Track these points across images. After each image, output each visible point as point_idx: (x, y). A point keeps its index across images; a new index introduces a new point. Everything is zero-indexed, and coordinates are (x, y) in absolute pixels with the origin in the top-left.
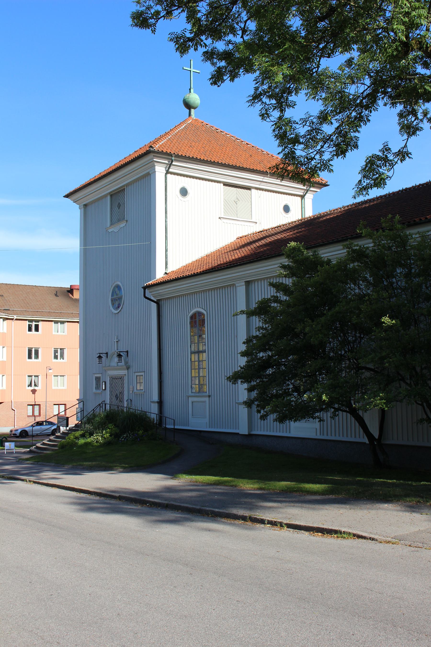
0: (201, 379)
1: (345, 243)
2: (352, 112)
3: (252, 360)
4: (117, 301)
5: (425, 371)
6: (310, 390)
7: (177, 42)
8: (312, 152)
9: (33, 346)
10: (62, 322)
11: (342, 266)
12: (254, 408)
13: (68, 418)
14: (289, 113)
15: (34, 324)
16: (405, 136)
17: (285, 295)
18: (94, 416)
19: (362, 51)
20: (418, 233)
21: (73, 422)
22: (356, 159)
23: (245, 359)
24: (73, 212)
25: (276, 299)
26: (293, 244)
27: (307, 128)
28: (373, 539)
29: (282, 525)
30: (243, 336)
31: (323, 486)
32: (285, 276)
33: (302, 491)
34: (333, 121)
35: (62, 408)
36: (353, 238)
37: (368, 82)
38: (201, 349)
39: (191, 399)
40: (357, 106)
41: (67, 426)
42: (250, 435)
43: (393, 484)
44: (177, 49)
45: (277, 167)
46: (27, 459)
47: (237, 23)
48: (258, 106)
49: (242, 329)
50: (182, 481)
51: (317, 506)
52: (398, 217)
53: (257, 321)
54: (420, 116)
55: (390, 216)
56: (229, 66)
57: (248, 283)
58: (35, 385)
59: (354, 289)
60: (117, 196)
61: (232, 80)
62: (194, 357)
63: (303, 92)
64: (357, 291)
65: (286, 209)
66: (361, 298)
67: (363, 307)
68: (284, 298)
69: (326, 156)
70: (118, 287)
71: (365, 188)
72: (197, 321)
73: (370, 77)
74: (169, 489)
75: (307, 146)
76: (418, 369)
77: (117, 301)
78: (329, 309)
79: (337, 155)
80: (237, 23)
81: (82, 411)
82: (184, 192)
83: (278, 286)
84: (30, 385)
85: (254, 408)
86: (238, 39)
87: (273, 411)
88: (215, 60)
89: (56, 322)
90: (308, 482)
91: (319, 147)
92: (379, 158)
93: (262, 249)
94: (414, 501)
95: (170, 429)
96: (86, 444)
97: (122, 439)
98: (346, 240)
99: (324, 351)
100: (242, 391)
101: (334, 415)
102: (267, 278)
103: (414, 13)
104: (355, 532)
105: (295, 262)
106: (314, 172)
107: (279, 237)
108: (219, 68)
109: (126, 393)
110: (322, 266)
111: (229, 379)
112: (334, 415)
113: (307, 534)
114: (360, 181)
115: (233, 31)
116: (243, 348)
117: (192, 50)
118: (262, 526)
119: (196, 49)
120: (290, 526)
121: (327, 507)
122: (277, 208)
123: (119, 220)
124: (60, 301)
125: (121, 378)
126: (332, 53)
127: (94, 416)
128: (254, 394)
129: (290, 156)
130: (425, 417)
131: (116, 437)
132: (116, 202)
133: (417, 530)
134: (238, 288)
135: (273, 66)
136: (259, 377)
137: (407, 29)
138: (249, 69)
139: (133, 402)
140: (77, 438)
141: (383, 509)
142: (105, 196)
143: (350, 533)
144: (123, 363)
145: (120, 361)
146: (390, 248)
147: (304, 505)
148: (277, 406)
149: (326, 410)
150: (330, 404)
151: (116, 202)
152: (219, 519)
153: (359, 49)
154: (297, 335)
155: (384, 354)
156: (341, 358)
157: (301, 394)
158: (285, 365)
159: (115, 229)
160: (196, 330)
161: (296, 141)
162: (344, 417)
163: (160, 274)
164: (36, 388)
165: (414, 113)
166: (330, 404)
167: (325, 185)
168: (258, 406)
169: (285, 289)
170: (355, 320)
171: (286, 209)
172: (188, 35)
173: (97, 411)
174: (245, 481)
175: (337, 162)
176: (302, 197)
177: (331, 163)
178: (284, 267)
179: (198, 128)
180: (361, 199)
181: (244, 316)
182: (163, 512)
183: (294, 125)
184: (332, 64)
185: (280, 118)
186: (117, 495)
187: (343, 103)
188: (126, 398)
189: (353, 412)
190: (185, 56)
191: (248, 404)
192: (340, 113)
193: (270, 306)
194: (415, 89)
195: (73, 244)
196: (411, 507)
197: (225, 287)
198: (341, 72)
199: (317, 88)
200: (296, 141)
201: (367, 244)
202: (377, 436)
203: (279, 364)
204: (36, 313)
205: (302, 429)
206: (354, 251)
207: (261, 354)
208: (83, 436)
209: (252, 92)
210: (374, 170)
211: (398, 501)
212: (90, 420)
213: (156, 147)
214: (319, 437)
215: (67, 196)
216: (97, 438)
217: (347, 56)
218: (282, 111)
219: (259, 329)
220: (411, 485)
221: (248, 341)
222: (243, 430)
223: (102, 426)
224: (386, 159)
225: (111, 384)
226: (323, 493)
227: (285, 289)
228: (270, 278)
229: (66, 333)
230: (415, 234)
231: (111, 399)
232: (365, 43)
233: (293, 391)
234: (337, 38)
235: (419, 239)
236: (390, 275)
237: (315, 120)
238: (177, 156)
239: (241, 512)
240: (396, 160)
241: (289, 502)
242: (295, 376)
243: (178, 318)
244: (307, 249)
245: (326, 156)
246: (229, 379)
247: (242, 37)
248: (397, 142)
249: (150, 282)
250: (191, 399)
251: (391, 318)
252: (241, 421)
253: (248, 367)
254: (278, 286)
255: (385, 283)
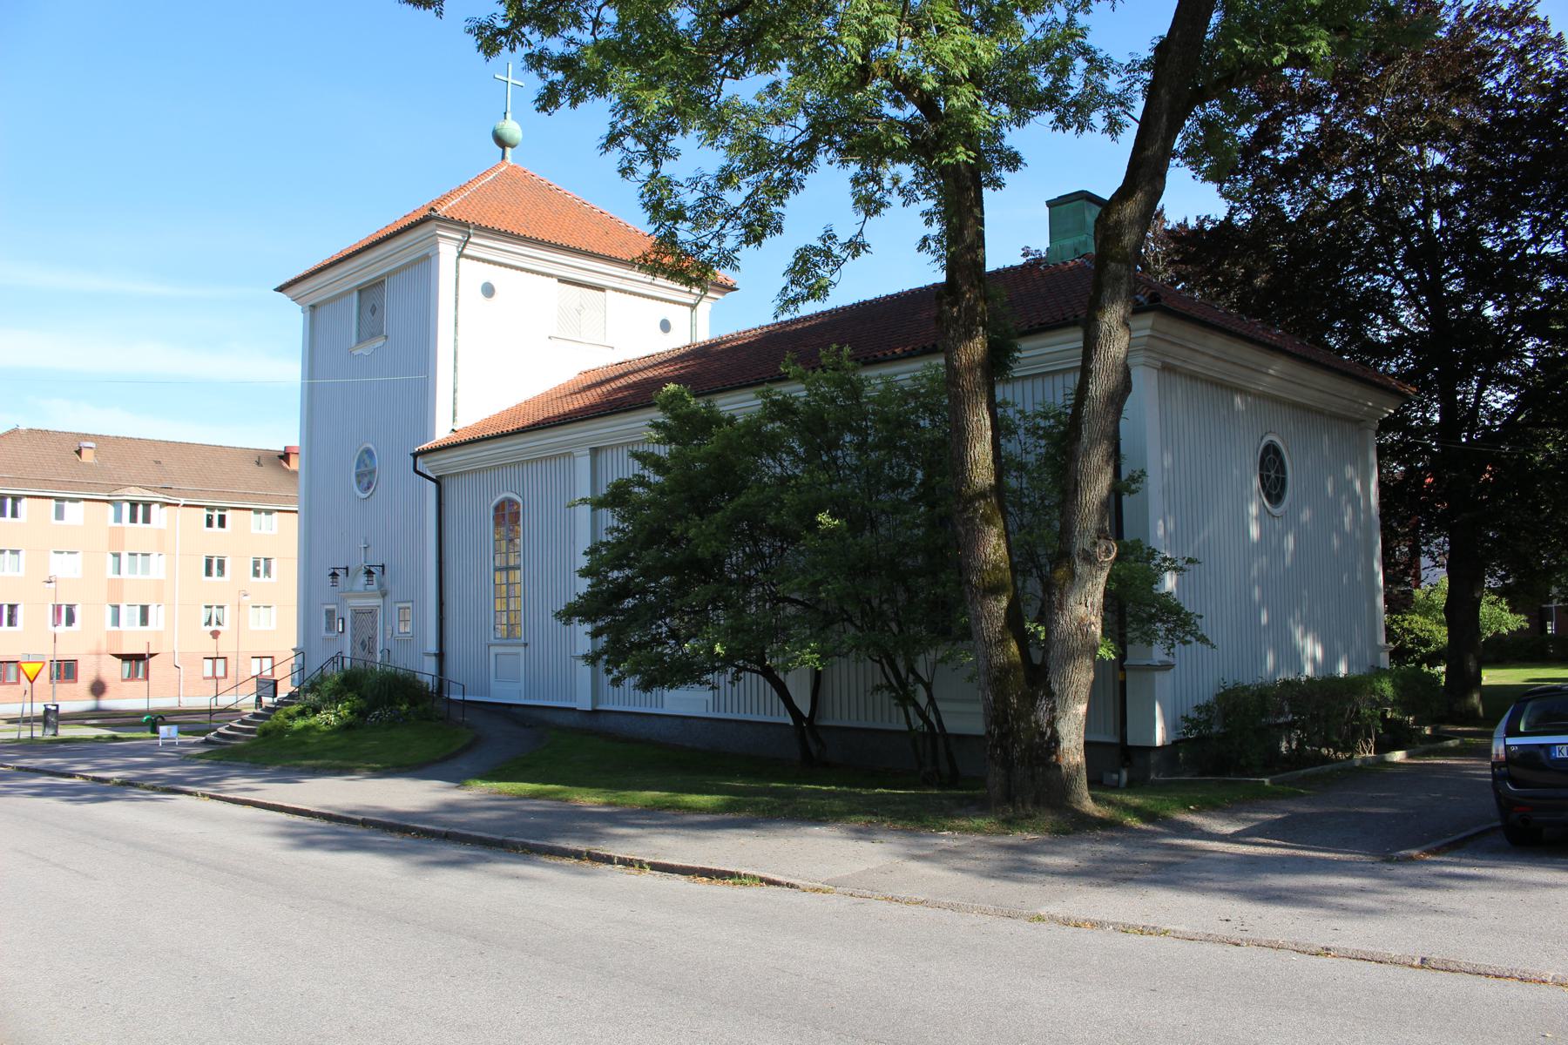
0: (512, 615)
1: (760, 389)
2: (777, 170)
3: (600, 583)
4: (366, 477)
5: (885, 606)
6: (695, 636)
7: (479, 35)
8: (705, 235)
9: (216, 553)
10: (269, 512)
11: (752, 429)
12: (601, 664)
13: (275, 682)
14: (667, 168)
15: (216, 514)
16: (863, 214)
17: (657, 473)
18: (323, 678)
19: (796, 72)
20: (880, 376)
21: (285, 689)
22: (777, 254)
23: (588, 581)
24: (292, 316)
25: (641, 481)
26: (672, 387)
27: (698, 194)
28: (792, 886)
29: (641, 865)
30: (584, 541)
31: (715, 797)
32: (658, 442)
33: (680, 808)
34: (743, 184)
35: (267, 663)
36: (772, 381)
37: (802, 122)
38: (512, 563)
39: (493, 650)
40: (782, 161)
41: (275, 695)
42: (595, 712)
43: (831, 792)
44: (480, 47)
45: (645, 257)
46: (200, 756)
47: (586, 10)
48: (616, 154)
49: (584, 530)
50: (476, 792)
51: (703, 833)
52: (847, 350)
53: (608, 518)
54: (887, 184)
55: (835, 346)
56: (571, 80)
57: (595, 452)
58: (218, 623)
59: (772, 468)
60: (370, 291)
61: (574, 104)
62: (501, 577)
63: (693, 134)
64: (778, 470)
65: (665, 326)
66: (783, 481)
67: (786, 498)
68: (654, 478)
69: (730, 243)
70: (368, 452)
71: (794, 301)
72: (506, 514)
73: (807, 114)
74: (452, 807)
75: (697, 226)
76: (875, 603)
77: (366, 477)
78: (731, 499)
79: (747, 242)
80: (586, 10)
81: (302, 669)
82: (488, 290)
83: (643, 458)
84: (209, 623)
85: (601, 664)
86: (586, 37)
87: (633, 672)
88: (545, 70)
89: (258, 511)
90: (690, 792)
91: (717, 227)
92: (817, 252)
93: (622, 395)
94: (860, 821)
95: (456, 702)
96: (307, 729)
97: (371, 719)
98: (762, 384)
99: (721, 570)
100: (581, 636)
101: (736, 679)
102: (627, 444)
103: (876, 20)
104: (763, 875)
105: (675, 417)
106: (706, 267)
107: (650, 374)
108: (552, 83)
109: (379, 638)
110: (719, 426)
111: (558, 615)
112: (736, 679)
113: (683, 879)
114: (785, 288)
115: (577, 21)
116: (583, 562)
117: (505, 50)
118: (609, 867)
119: (512, 49)
120: (655, 867)
121: (719, 833)
122: (648, 324)
123: (373, 336)
124: (267, 474)
125: (371, 612)
126: (743, 71)
127: (323, 678)
128: (603, 640)
129: (668, 241)
130: (884, 681)
131: (371, 717)
132: (368, 302)
133: (864, 868)
134: (578, 460)
135: (641, 88)
136: (612, 613)
137: (865, 45)
138: (602, 90)
139: (393, 655)
140: (291, 717)
141: (811, 835)
142: (349, 292)
143: (754, 877)
144: (375, 586)
145: (369, 582)
146: (833, 400)
147: (682, 831)
148: (639, 664)
149: (722, 670)
150: (728, 660)
151: (368, 302)
152: (536, 857)
153: (790, 68)
154: (675, 542)
155: (819, 577)
156: (748, 583)
157: (680, 642)
158: (654, 593)
159: (365, 350)
160: (503, 530)
161: (678, 215)
162: (753, 682)
163: (442, 432)
164: (219, 628)
165: (876, 178)
166: (728, 660)
167: (732, 289)
168: (608, 662)
169: (658, 464)
170: (772, 519)
171: (665, 326)
172: (500, 24)
173: (329, 670)
174: (584, 790)
175: (747, 254)
176: (693, 307)
177: (737, 254)
178: (656, 426)
179: (517, 181)
180: (786, 317)
181: (588, 508)
182: (438, 847)
183: (676, 189)
184: (744, 89)
185: (653, 176)
186: (360, 818)
187: (759, 156)
188: (379, 647)
189: (768, 673)
190: (493, 59)
191: (592, 659)
192: (755, 171)
193: (630, 493)
194: (877, 140)
195: (288, 371)
196: (858, 831)
197: (555, 457)
198: (758, 104)
199: (716, 128)
200: (678, 215)
201: (796, 391)
202: (806, 714)
203: (644, 591)
204: (221, 494)
205: (684, 701)
206: (774, 403)
207: (616, 574)
208: (302, 713)
209: (606, 130)
210: (807, 268)
211: (837, 821)
212: (316, 687)
213: (442, 211)
214: (711, 714)
215: (280, 289)
216: (328, 718)
217: (766, 79)
218: (656, 164)
219: (611, 530)
220: (860, 795)
221: (593, 551)
222: (584, 703)
223: (337, 696)
224: (828, 254)
225: (353, 623)
226: (713, 811)
227: (658, 464)
228: (633, 443)
229: (275, 531)
230: (875, 378)
231: (353, 648)
232: (799, 57)
233: (668, 637)
234: (752, 47)
235: (881, 387)
236: (833, 445)
237: (711, 182)
238: (479, 228)
239: (573, 845)
240: (844, 255)
241: (656, 826)
242: (671, 612)
243: (473, 510)
244: (696, 396)
245: (730, 243)
246: (558, 615)
247: (593, 33)
248: (847, 224)
249: (425, 446)
250: (493, 650)
251: (833, 516)
252: (579, 688)
253: (591, 596)
254: (643, 458)
255: (825, 458)
